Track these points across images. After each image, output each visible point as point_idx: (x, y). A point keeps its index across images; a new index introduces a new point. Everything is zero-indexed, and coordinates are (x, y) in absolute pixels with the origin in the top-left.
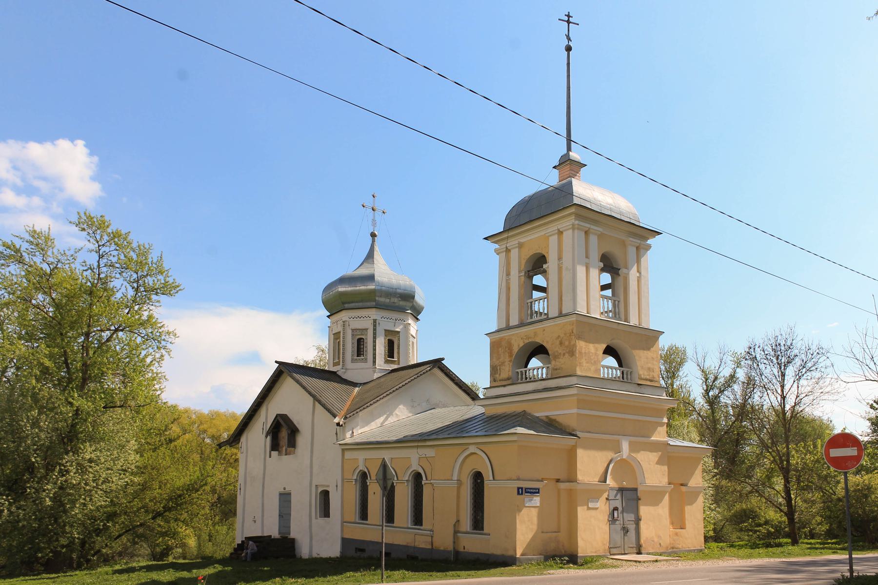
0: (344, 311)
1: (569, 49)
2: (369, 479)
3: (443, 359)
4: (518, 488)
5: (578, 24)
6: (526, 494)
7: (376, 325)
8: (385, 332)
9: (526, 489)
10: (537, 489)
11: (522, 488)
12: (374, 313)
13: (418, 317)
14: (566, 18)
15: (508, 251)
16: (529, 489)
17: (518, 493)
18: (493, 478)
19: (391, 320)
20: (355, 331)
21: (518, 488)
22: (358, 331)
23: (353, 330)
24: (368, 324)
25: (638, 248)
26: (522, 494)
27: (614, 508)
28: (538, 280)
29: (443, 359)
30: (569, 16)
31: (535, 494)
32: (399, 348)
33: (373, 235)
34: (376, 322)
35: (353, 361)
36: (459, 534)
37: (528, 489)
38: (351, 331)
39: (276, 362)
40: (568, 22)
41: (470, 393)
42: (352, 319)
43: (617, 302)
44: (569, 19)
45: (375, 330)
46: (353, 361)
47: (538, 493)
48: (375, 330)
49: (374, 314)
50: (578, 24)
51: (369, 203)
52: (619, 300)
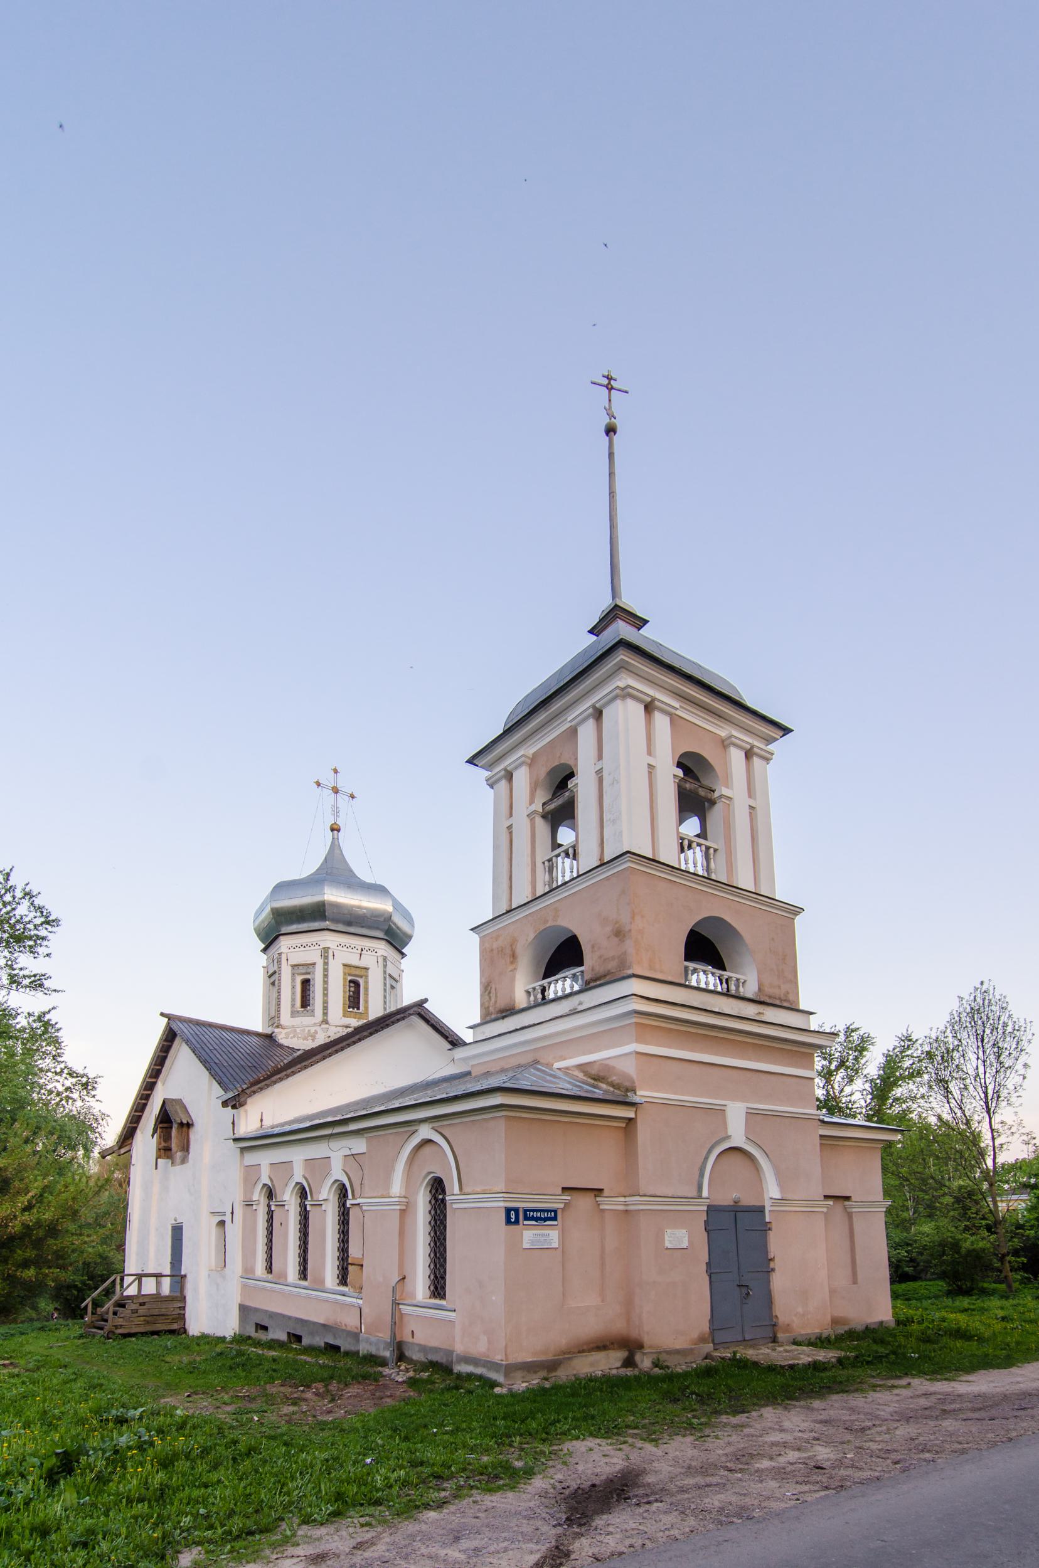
0: (634, 980)
1: (610, 430)
2: (309, 1198)
3: (426, 1000)
4: (508, 1210)
5: (627, 392)
6: (525, 1223)
7: (327, 956)
8: (344, 969)
9: (525, 1211)
10: (551, 1211)
11: (516, 1210)
12: (383, 947)
13: (403, 951)
14: (605, 382)
15: (509, 776)
16: (533, 1211)
17: (508, 1221)
18: (461, 1188)
19: (355, 950)
20: (296, 968)
21: (508, 1210)
22: (301, 967)
23: (293, 966)
24: (314, 956)
25: (749, 754)
26: (517, 1222)
27: (707, 1354)
28: (565, 836)
29: (426, 1000)
30: (609, 378)
31: (548, 1223)
32: (366, 994)
33: (335, 829)
34: (328, 953)
35: (294, 1014)
36: (401, 1306)
37: (530, 1211)
38: (290, 968)
39: (162, 1014)
40: (610, 388)
41: (455, 1042)
42: (292, 949)
43: (712, 851)
44: (609, 383)
45: (326, 964)
46: (294, 1014)
47: (555, 1219)
48: (326, 964)
49: (330, 940)
50: (627, 392)
51: (328, 779)
52: (716, 847)
